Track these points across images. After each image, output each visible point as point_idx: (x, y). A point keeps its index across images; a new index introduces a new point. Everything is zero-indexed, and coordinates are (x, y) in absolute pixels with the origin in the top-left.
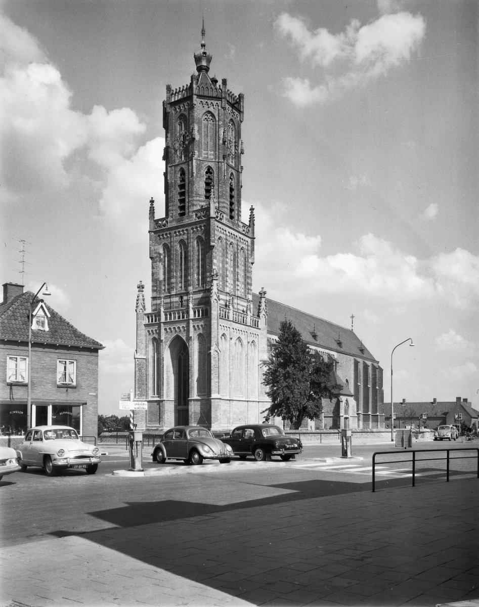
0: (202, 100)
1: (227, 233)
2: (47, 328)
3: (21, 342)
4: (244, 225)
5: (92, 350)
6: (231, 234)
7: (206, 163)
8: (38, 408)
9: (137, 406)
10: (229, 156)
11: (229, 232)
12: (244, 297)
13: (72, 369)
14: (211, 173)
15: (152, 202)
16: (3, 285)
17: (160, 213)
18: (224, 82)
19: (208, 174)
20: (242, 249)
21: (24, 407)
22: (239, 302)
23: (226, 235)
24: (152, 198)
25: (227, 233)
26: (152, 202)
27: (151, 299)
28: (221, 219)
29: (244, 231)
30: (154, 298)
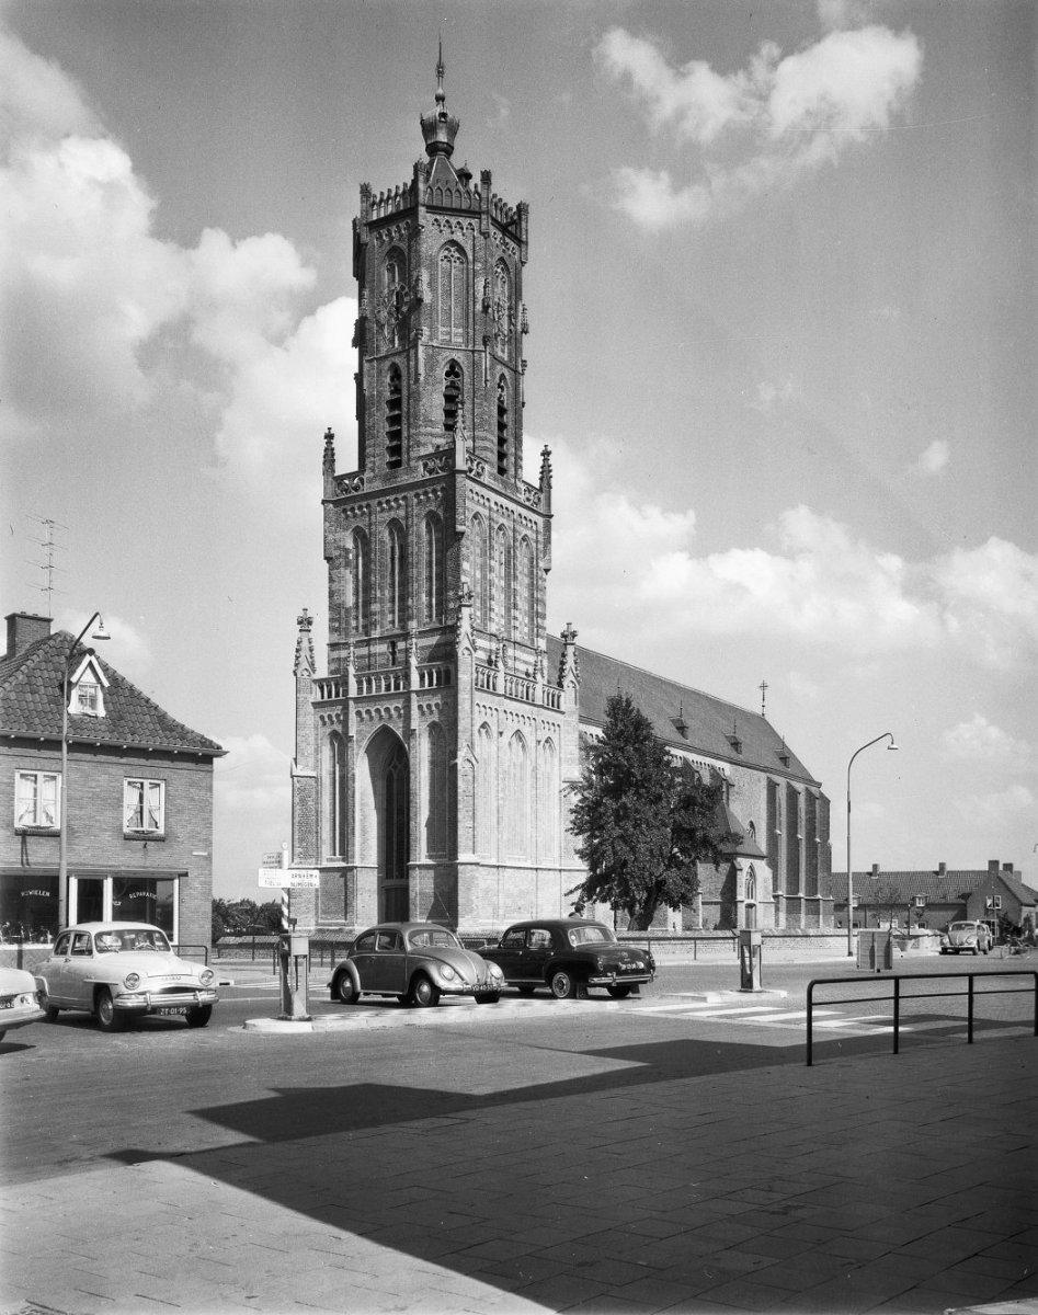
0: (438, 217)
1: (493, 505)
2: (101, 712)
3: (46, 740)
4: (530, 488)
5: (199, 757)
6: (502, 506)
7: (447, 353)
8: (82, 884)
9: (297, 880)
10: (496, 338)
11: (496, 503)
12: (529, 644)
13: (155, 799)
14: (457, 375)
15: (329, 437)
16: (6, 618)
17: (347, 462)
18: (486, 177)
19: (452, 378)
20: (524, 539)
21: (51, 882)
22: (518, 654)
23: (490, 509)
24: (329, 429)
25: (493, 505)
26: (329, 437)
27: (326, 648)
28: (479, 474)
29: (528, 500)
30: (333, 646)
